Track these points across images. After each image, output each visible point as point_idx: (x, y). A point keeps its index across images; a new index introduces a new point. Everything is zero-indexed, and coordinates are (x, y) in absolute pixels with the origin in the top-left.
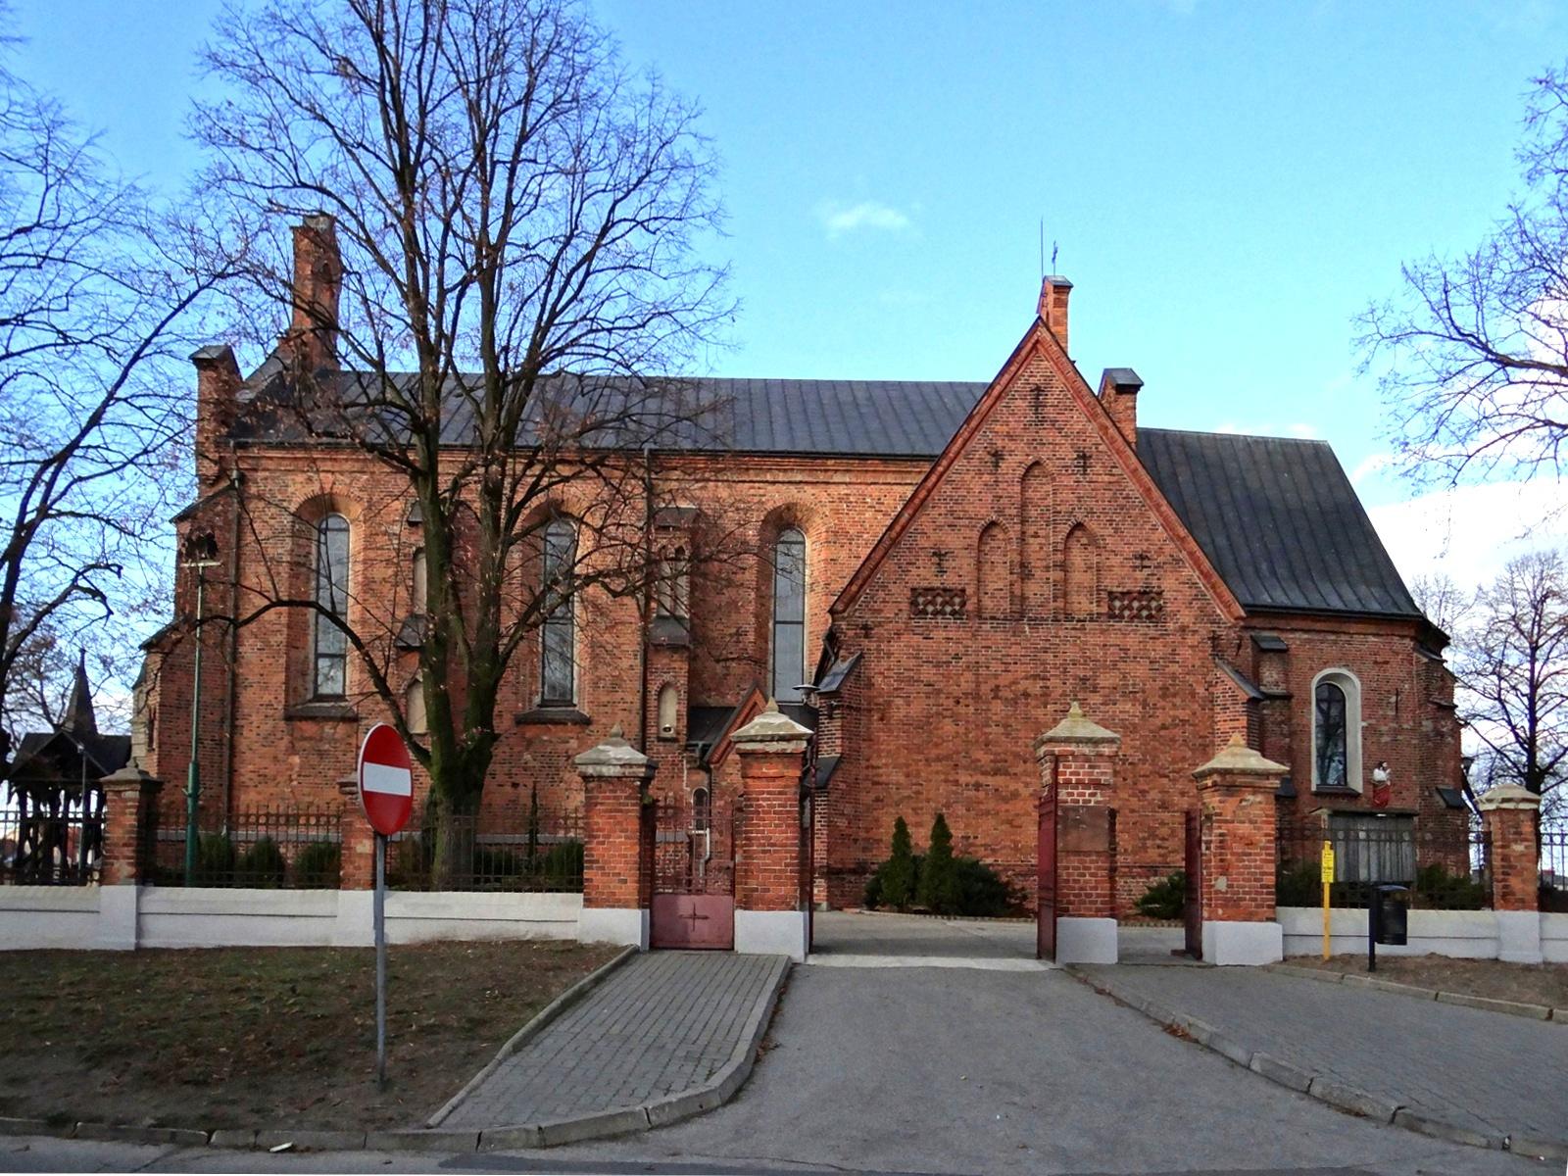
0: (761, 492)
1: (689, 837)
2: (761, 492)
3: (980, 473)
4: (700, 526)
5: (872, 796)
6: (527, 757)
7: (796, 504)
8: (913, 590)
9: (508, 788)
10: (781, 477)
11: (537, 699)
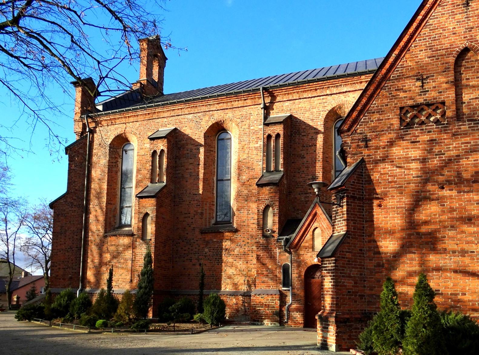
0: (324, 101)
1: (280, 291)
2: (324, 101)
3: (454, 14)
4: (291, 124)
5: (374, 262)
6: (206, 250)
7: (343, 105)
8: (401, 108)
9: (198, 267)
10: (335, 90)
11: (213, 221)
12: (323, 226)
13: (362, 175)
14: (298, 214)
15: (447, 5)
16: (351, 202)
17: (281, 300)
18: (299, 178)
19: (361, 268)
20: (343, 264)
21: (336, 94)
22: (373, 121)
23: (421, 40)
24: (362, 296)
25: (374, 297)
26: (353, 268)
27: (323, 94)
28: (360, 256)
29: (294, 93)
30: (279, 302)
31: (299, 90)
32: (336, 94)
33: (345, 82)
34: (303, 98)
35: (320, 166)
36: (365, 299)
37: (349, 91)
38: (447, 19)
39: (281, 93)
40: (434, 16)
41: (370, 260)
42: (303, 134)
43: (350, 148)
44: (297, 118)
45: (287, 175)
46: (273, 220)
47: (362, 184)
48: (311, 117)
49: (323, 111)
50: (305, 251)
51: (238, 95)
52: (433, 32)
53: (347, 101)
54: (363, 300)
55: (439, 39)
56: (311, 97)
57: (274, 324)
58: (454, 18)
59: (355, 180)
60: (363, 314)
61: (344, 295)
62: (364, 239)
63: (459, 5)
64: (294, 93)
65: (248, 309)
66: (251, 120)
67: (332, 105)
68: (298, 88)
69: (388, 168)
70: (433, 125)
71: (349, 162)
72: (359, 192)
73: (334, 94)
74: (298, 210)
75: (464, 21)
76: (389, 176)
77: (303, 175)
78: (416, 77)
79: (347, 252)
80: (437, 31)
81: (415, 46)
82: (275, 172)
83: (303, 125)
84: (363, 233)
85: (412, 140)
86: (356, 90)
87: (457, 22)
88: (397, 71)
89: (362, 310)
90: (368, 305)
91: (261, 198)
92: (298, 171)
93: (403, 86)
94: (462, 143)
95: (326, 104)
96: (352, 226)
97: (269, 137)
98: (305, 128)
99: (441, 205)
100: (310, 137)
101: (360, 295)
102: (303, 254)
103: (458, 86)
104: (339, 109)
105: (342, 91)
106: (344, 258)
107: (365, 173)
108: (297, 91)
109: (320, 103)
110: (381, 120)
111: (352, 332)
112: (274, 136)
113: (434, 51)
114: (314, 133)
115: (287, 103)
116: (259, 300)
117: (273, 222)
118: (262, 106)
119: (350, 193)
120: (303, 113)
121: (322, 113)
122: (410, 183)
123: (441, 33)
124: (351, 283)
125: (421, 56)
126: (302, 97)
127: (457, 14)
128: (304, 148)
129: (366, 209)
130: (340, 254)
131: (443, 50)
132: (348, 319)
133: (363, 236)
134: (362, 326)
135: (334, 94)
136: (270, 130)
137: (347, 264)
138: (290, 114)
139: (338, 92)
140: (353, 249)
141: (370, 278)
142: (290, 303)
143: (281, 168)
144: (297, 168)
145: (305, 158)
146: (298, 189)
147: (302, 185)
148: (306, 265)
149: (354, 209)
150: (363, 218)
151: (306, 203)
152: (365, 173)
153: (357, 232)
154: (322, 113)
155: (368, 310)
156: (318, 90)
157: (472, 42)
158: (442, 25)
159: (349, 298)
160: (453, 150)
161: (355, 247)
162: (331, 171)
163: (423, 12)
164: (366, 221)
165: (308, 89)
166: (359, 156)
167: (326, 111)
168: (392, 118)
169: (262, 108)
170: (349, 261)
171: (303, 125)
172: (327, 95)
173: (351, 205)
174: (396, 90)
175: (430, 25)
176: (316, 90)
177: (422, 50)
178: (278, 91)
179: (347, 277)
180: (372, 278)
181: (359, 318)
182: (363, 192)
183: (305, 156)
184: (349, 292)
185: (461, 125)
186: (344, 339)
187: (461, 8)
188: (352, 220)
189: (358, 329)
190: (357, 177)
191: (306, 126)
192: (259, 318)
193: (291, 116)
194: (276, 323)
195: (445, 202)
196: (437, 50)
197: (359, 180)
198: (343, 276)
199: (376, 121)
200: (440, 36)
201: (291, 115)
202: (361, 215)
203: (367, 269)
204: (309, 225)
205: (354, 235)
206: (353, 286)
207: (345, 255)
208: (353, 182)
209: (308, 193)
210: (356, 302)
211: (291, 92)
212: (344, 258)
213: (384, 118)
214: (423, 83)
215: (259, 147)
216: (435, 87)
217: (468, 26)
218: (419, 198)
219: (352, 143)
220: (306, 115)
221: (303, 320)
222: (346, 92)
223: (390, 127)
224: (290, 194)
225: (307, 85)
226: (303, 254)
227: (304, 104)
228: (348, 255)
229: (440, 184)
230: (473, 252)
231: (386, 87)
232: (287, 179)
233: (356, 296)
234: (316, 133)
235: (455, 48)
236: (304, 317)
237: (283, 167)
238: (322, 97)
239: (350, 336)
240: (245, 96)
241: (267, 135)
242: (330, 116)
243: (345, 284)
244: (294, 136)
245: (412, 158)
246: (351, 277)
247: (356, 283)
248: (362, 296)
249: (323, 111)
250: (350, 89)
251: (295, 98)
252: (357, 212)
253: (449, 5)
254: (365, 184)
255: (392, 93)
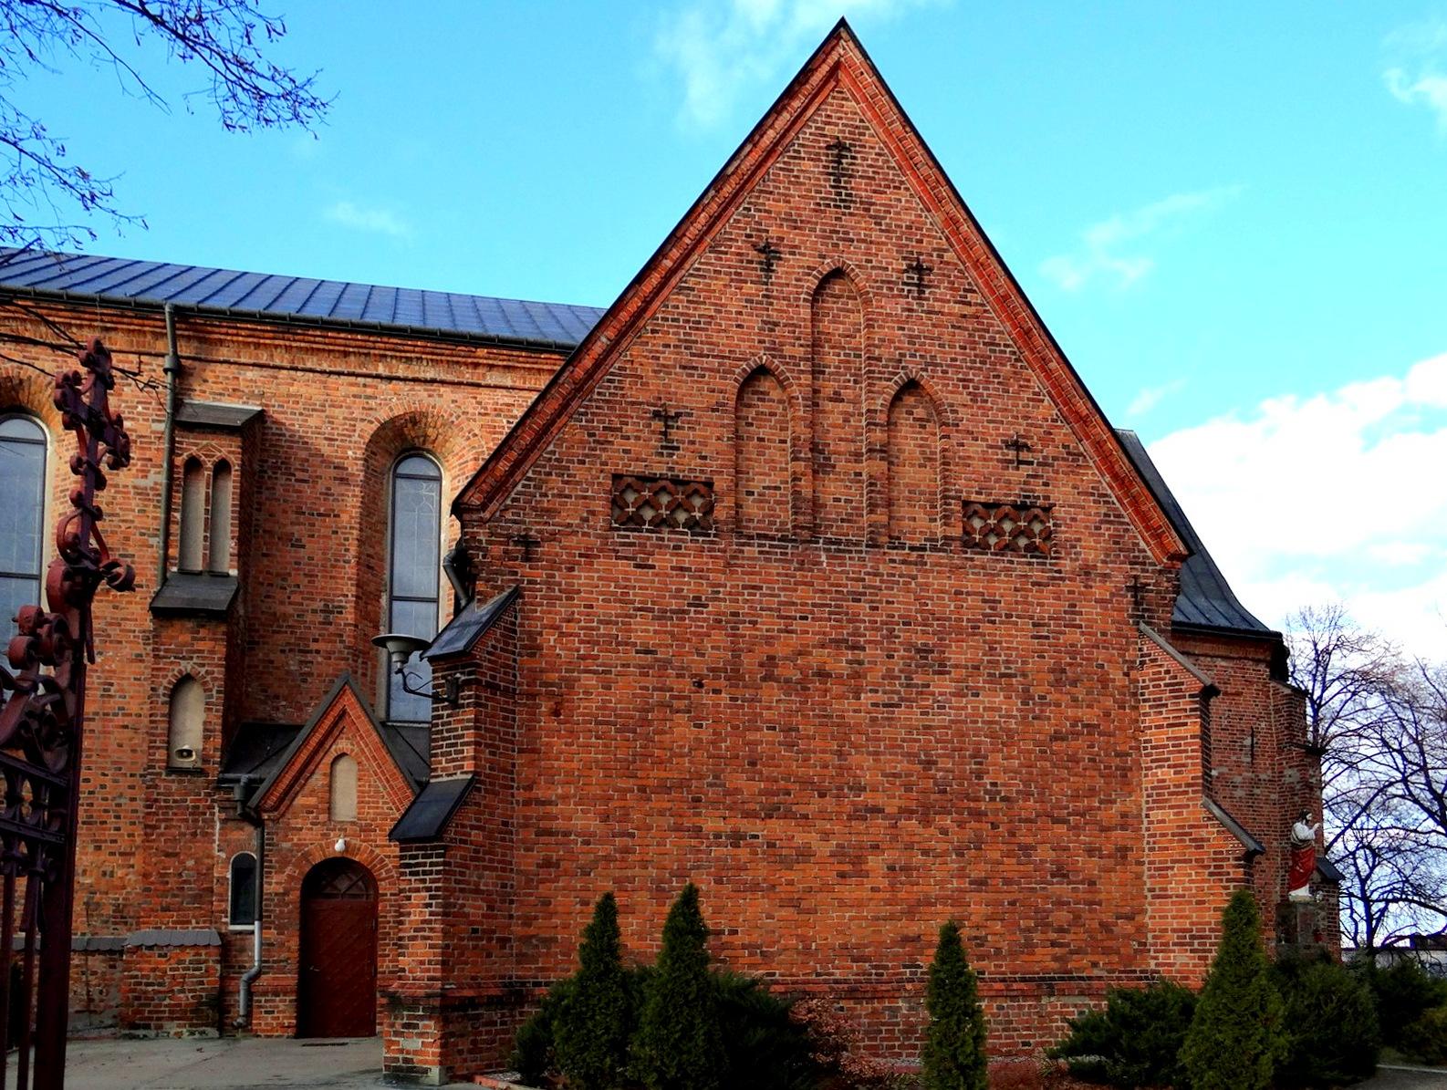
0: (369, 391)
2: (369, 391)
7: (424, 415)
8: (617, 477)
10: (401, 370)
12: (362, 750)
13: (515, 632)
14: (278, 709)
15: (726, 253)
16: (487, 699)
17: (226, 961)
18: (282, 603)
19: (504, 870)
20: (462, 857)
21: (405, 380)
22: (546, 495)
23: (667, 320)
24: (504, 942)
25: (534, 941)
26: (485, 868)
27: (364, 371)
28: (503, 840)
29: (277, 346)
30: (218, 967)
31: (294, 344)
32: (405, 380)
33: (433, 354)
34: (303, 370)
35: (350, 579)
36: (511, 947)
37: (443, 382)
38: (725, 286)
39: (235, 338)
40: (699, 270)
41: (527, 850)
42: (299, 475)
43: (484, 557)
44: (284, 424)
45: (246, 592)
46: (205, 723)
47: (514, 653)
48: (327, 429)
49: (363, 420)
50: (305, 819)
51: (82, 308)
52: (695, 309)
53: (434, 407)
54: (507, 951)
55: (707, 330)
56: (331, 373)
57: (201, 1033)
58: (741, 288)
59: (497, 641)
60: (505, 985)
61: (462, 939)
62: (513, 795)
63: (751, 262)
64: (277, 346)
65: (101, 992)
66: (124, 398)
67: (391, 410)
68: (291, 337)
69: (580, 621)
70: (686, 534)
71: (480, 593)
72: (505, 673)
73: (398, 379)
74: (277, 697)
75: (761, 303)
76: (581, 642)
77: (296, 598)
78: (652, 409)
79: (473, 827)
80: (702, 310)
81: (653, 331)
82: (206, 577)
83: (298, 448)
84: (513, 780)
85: (638, 561)
86: (460, 384)
87: (747, 301)
88: (609, 381)
89: (502, 977)
90: (518, 963)
91: (166, 651)
92: (280, 582)
93: (622, 423)
94: (744, 587)
95: (372, 403)
96: (486, 760)
97: (193, 465)
98: (307, 460)
99: (695, 726)
100: (321, 487)
101: (499, 939)
102: (301, 829)
103: (741, 452)
104: (410, 425)
105: (422, 376)
106: (465, 842)
107: (522, 625)
108: (287, 343)
109: (354, 396)
110: (566, 496)
111: (480, 1033)
112: (209, 465)
113: (694, 355)
114: (335, 479)
115: (251, 374)
116: (149, 962)
117: (205, 730)
118: (167, 362)
119: (484, 674)
120: (301, 414)
121: (359, 425)
122: (629, 666)
123: (711, 317)
124: (480, 908)
125: (665, 358)
126: (301, 366)
127: (746, 282)
128: (302, 518)
129: (521, 719)
130: (456, 833)
131: (714, 357)
132: (472, 999)
133: (512, 787)
134: (503, 1015)
135: (398, 379)
136: (196, 445)
137: (472, 859)
138: (259, 408)
139: (410, 376)
140: (487, 821)
141: (526, 895)
142: (254, 970)
143: (232, 567)
144: (278, 575)
145: (303, 547)
146: (279, 636)
147: (290, 627)
148: (308, 861)
149: (493, 716)
150: (513, 743)
151: (305, 681)
152: (522, 625)
153: (497, 777)
154: (359, 425)
155: (517, 977)
156: (352, 358)
157: (774, 357)
158: (715, 298)
159: (475, 947)
160: (725, 600)
161: (492, 814)
162: (380, 597)
163: (675, 253)
164: (521, 751)
165: (321, 346)
166: (510, 581)
167: (371, 422)
168: (593, 498)
169: (166, 371)
170: (476, 851)
171: (302, 449)
172: (378, 377)
173: (486, 706)
174: (605, 429)
175: (688, 288)
176: (346, 354)
177: (669, 346)
178: (224, 330)
179: (471, 891)
180: (531, 895)
181: (497, 996)
182: (514, 676)
183: (304, 541)
184: (475, 931)
185: (744, 544)
186: (460, 1052)
187: (756, 269)
188: (487, 746)
189: (495, 1023)
190: (502, 635)
191: (311, 455)
192: (151, 1019)
193: (261, 416)
194: (208, 1029)
195: (703, 719)
196: (701, 355)
197: (507, 644)
198: (462, 890)
199: (553, 495)
200: (710, 323)
201: (263, 411)
202: (507, 733)
203: (520, 872)
204: (321, 744)
205: (491, 784)
206: (483, 915)
207: (470, 835)
208: (493, 646)
209: (311, 652)
210: (489, 955)
211: (268, 341)
212: (465, 842)
213: (573, 494)
214: (667, 427)
215: (152, 489)
216: (693, 443)
217: (768, 316)
218: (648, 703)
219: (489, 542)
220: (313, 422)
221: (296, 1018)
222: (433, 381)
223: (587, 520)
224: (253, 649)
225: (318, 333)
226: (301, 829)
227: (306, 387)
228: (476, 836)
229: (696, 675)
230: (756, 837)
231: (582, 414)
232: (245, 602)
233: (490, 940)
234: (342, 479)
235: (740, 360)
236: (297, 1007)
237: (235, 564)
238: (361, 380)
239: (474, 1042)
240: (106, 318)
241: (185, 455)
242: (384, 439)
243: (466, 910)
244: (270, 477)
245: (637, 605)
246: (482, 892)
247: (491, 908)
248: (504, 942)
249: (363, 420)
250: (443, 376)
251: (278, 362)
252: (502, 725)
253: (732, 253)
254: (520, 654)
255: (594, 435)
